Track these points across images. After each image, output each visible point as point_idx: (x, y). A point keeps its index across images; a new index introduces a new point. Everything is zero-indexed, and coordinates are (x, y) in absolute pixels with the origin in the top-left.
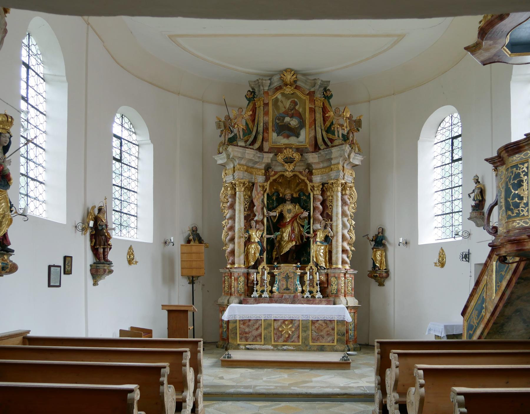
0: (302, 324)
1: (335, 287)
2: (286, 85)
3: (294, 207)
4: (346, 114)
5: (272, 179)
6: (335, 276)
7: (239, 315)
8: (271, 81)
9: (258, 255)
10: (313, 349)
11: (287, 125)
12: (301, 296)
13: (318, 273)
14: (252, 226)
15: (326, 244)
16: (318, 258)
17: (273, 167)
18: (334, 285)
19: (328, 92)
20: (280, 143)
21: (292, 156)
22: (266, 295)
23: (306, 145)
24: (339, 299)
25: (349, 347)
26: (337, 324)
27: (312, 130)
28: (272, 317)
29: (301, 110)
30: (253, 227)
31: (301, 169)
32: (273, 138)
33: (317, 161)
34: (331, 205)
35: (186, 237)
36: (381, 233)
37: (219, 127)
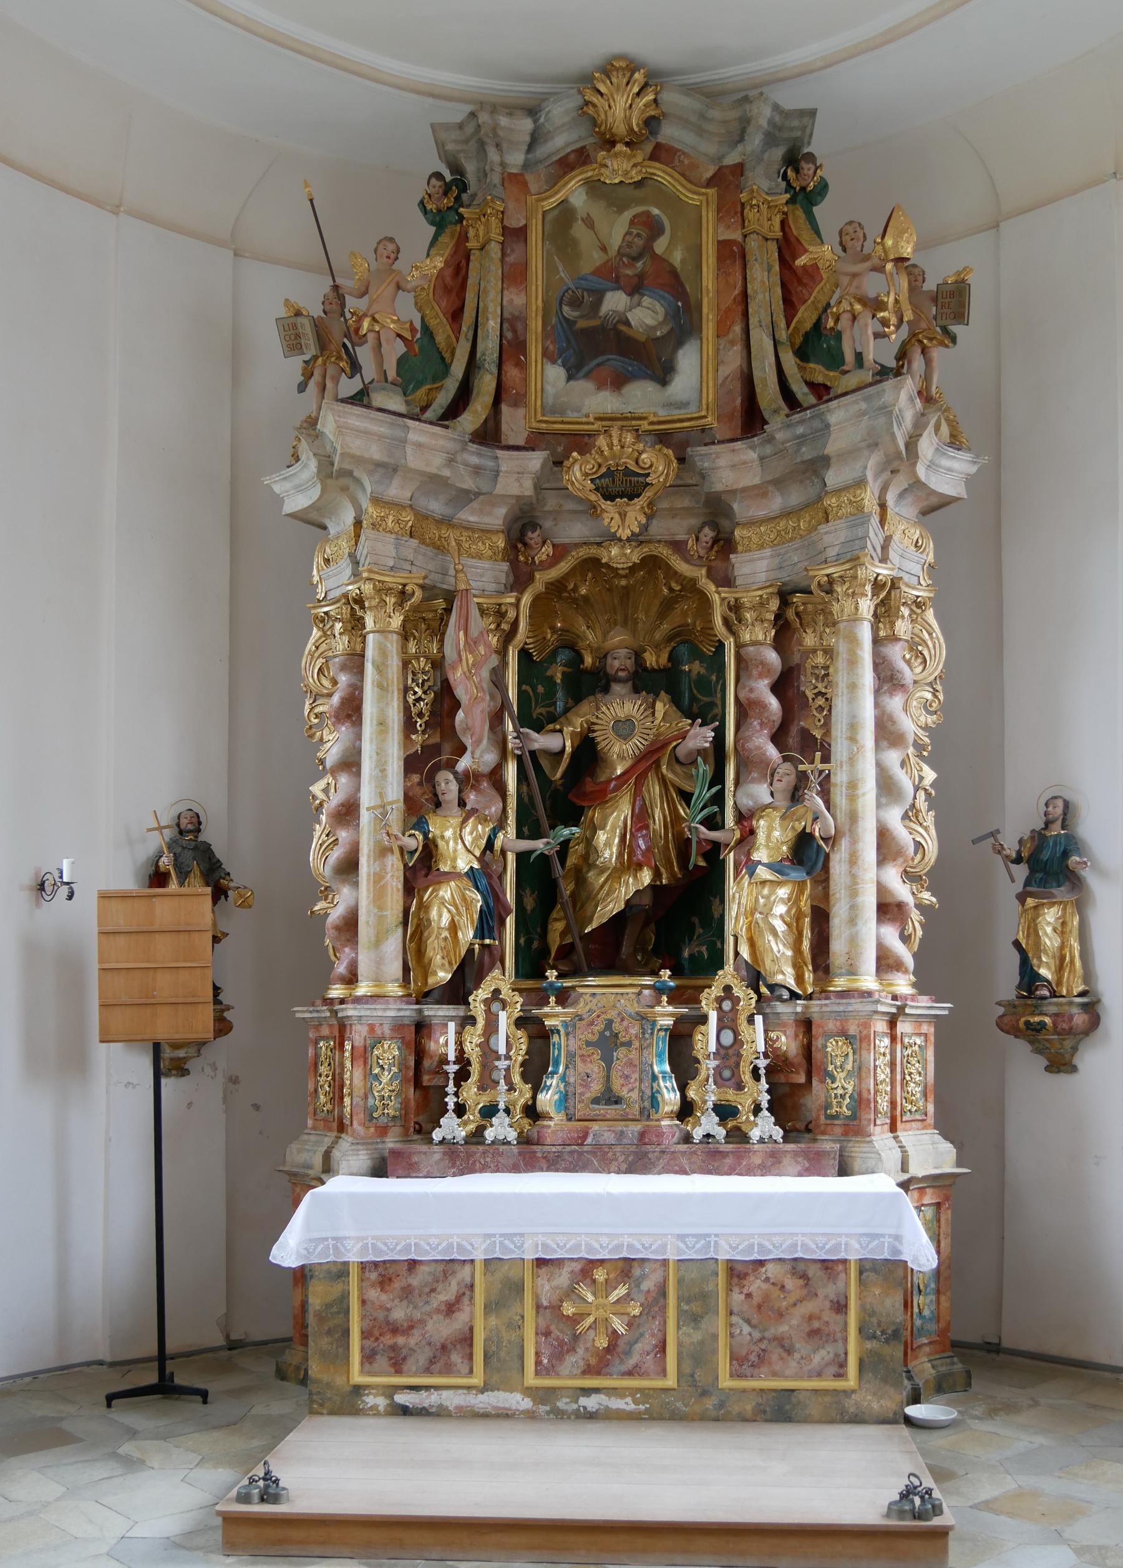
0: (680, 1281)
1: (843, 1084)
2: (609, 143)
3: (645, 710)
4: (896, 244)
5: (542, 579)
6: (843, 1033)
7: (359, 1239)
8: (535, 121)
9: (471, 934)
10: (736, 1409)
11: (615, 328)
12: (677, 1135)
13: (759, 1019)
14: (441, 797)
15: (798, 875)
16: (759, 943)
17: (547, 524)
18: (843, 1075)
19: (807, 168)
20: (579, 411)
21: (637, 463)
22: (500, 1129)
23: (705, 417)
24: (864, 1148)
25: (917, 1380)
26: (861, 1282)
27: (732, 343)
28: (526, 1246)
29: (677, 258)
30: (448, 802)
31: (679, 528)
32: (549, 389)
33: (757, 481)
34: (823, 690)
35: (148, 859)
36: (1059, 822)
37: (293, 344)
